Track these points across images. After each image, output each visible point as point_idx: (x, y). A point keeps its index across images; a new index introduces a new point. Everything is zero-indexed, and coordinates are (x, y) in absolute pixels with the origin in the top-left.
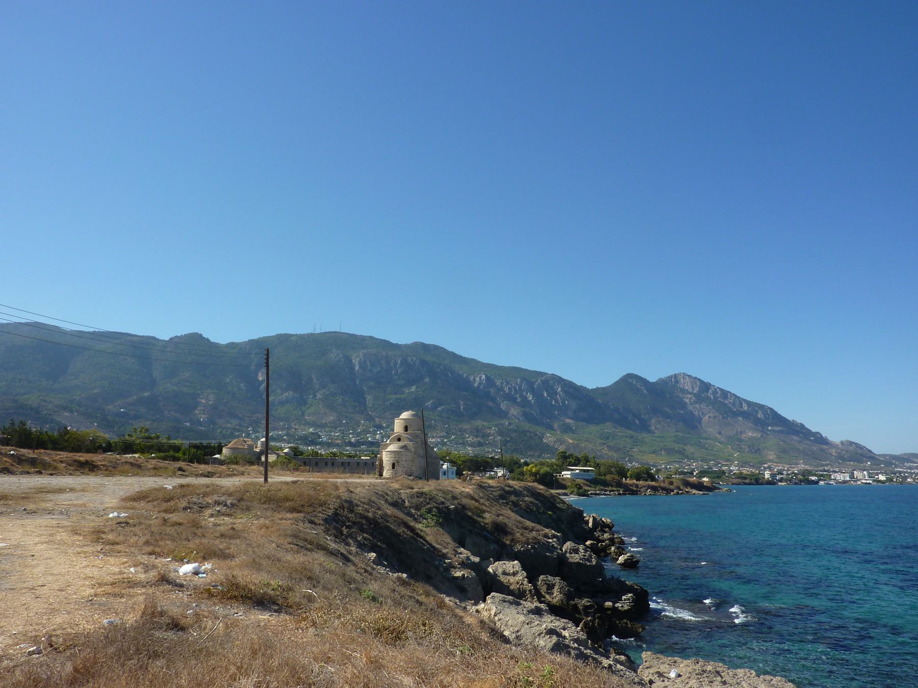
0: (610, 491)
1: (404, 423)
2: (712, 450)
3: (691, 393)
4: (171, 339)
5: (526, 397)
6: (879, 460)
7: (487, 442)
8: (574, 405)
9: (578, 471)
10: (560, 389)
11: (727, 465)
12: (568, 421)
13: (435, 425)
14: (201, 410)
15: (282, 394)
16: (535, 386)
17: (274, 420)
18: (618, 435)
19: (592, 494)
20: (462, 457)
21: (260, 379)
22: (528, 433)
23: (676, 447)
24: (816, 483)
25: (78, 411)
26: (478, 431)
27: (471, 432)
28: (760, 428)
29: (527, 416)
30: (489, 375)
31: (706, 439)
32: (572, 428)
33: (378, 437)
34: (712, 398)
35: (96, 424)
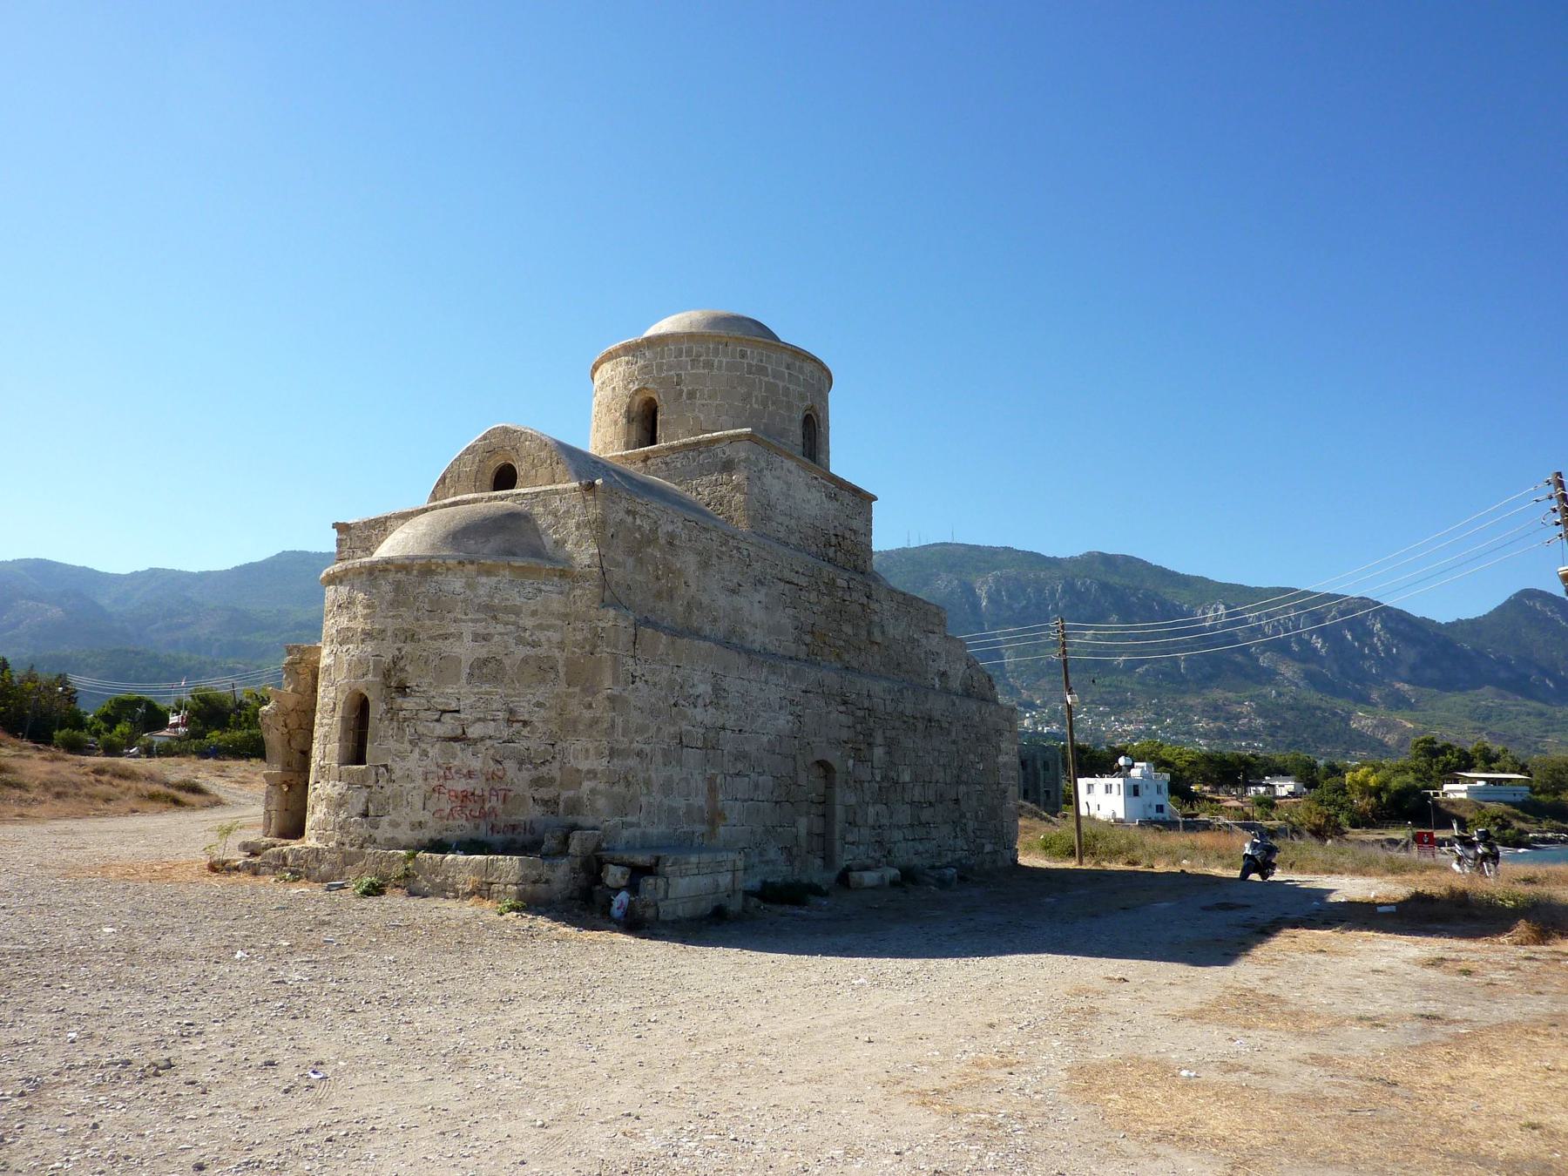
1: (628, 380)
5: (1308, 642)
7: (1236, 729)
8: (1411, 655)
9: (1481, 783)
10: (1379, 626)
13: (1133, 699)
20: (1187, 753)
26: (1216, 708)
27: (1203, 711)
32: (1409, 700)
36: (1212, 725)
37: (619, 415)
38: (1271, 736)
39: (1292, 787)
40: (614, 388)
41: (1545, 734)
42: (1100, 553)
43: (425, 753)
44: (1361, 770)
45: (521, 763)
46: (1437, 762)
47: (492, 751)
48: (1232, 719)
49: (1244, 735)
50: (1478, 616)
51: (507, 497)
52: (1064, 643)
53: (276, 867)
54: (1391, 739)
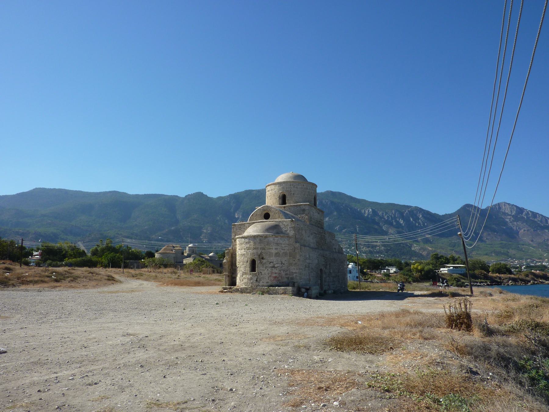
0: (480, 283)
1: (280, 190)
2: (528, 252)
3: (510, 215)
4: (186, 196)
7: (375, 251)
9: (451, 268)
10: (421, 216)
11: (540, 261)
14: (204, 236)
16: (405, 215)
21: (237, 217)
22: (401, 244)
30: (374, 209)
31: (523, 245)
34: (525, 218)
36: (367, 249)
37: (277, 197)
38: (386, 253)
39: (395, 270)
40: (275, 191)
41: (472, 251)
42: (330, 191)
43: (268, 270)
44: (416, 264)
45: (284, 271)
46: (439, 261)
47: (279, 269)
48: (374, 247)
49: (378, 252)
50: (452, 213)
51: (273, 221)
52: (356, 239)
53: (236, 291)
54: (424, 253)
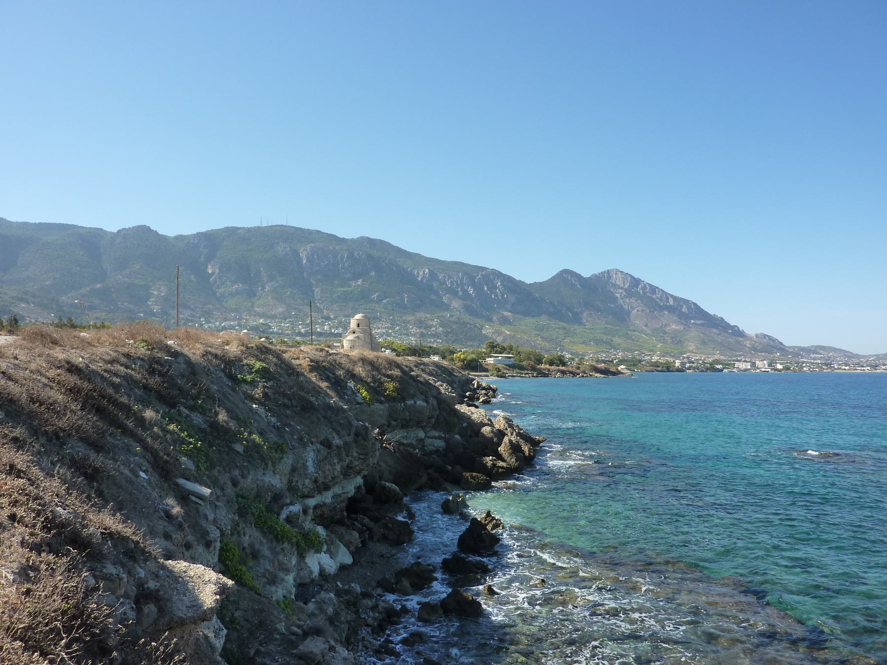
0: (525, 374)
3: (622, 288)
5: (467, 290)
6: (788, 351)
8: (512, 299)
12: (506, 313)
14: (153, 302)
15: (232, 286)
17: (225, 311)
18: (552, 327)
19: (509, 376)
23: (605, 338)
24: (721, 370)
25: (33, 303)
28: (684, 322)
29: (469, 310)
33: (326, 328)
35: (53, 315)
